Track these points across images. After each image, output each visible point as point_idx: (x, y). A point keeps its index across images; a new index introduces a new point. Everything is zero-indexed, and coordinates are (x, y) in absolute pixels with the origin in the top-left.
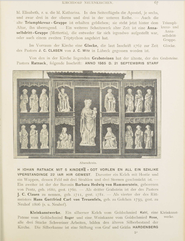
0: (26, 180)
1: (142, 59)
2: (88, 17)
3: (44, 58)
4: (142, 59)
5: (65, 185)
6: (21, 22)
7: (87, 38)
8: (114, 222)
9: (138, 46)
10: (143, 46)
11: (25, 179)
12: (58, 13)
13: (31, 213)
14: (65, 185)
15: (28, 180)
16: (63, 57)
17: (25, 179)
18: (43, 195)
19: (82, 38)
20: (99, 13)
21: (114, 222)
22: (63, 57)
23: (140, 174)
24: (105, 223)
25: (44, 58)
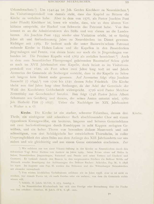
0: (15, 107)
1: (79, 65)
2: (22, 125)
3: (40, 18)
4: (79, 65)
5: (93, 78)
6: (77, 47)
7: (59, 14)
8: (113, 22)
9: (76, 57)
10: (66, 10)
11: (15, 106)
12: (70, 184)
13: (22, 113)
14: (93, 78)
15: (17, 107)
16: (27, 47)
17: (15, 106)
18: (71, 40)
19: (73, 142)
20: (63, 86)
21: (113, 22)
22: (27, 47)
23: (19, 101)
24: (104, 48)
25: (40, 18)
